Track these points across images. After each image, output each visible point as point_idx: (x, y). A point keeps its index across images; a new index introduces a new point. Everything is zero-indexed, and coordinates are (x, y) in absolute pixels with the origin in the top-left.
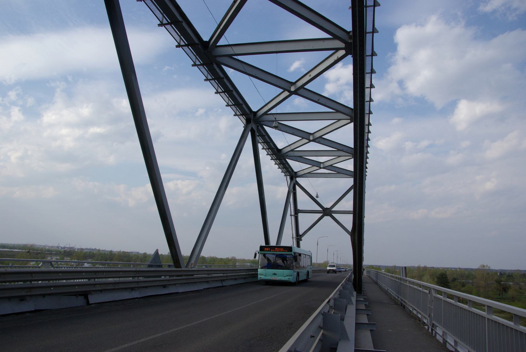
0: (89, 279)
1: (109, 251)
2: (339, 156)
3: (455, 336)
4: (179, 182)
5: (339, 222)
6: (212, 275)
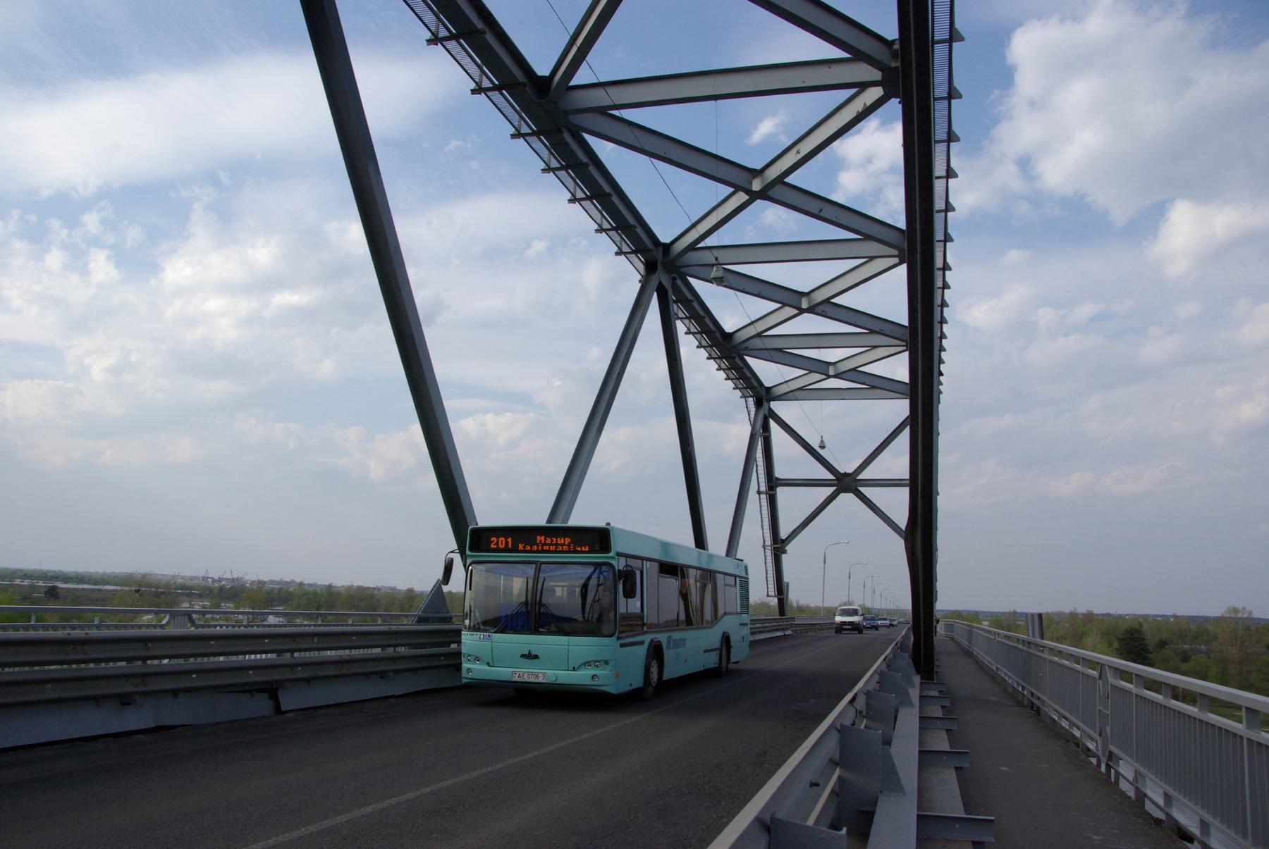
0: (280, 652)
2: (874, 347)
4: (489, 418)
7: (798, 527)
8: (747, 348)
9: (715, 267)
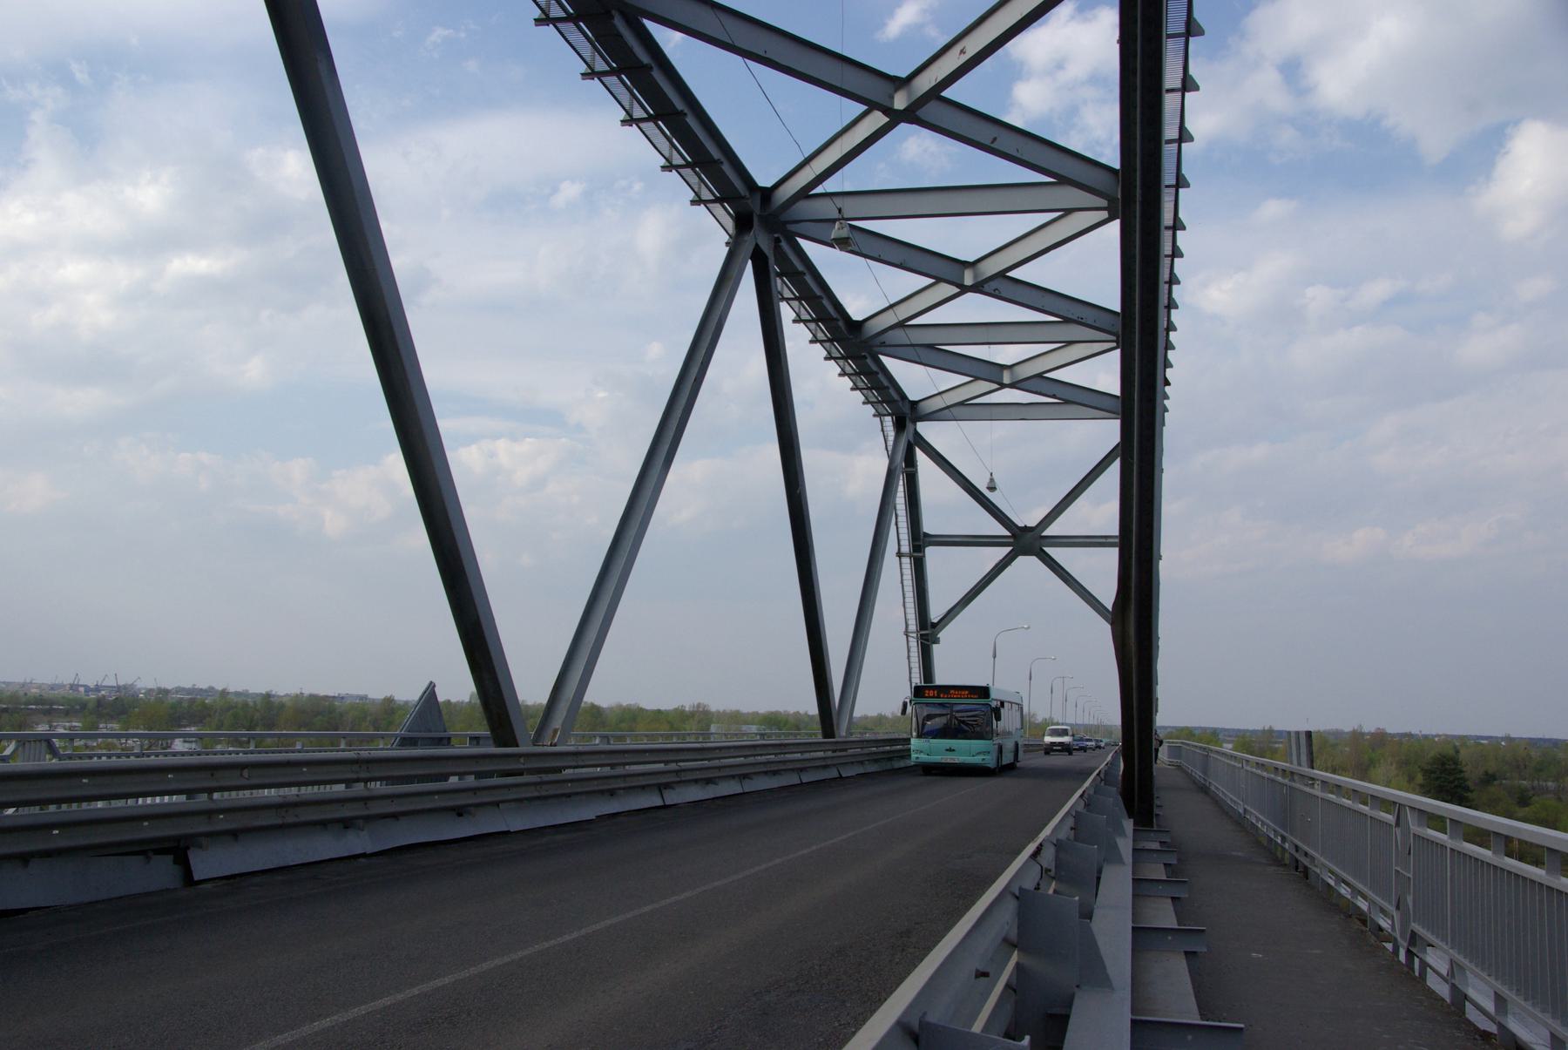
1: (261, 694)
2: (1070, 343)
3: (1496, 979)
4: (502, 445)
5: (1070, 576)
6: (627, 767)
7: (957, 604)
8: (883, 344)
9: (837, 223)
